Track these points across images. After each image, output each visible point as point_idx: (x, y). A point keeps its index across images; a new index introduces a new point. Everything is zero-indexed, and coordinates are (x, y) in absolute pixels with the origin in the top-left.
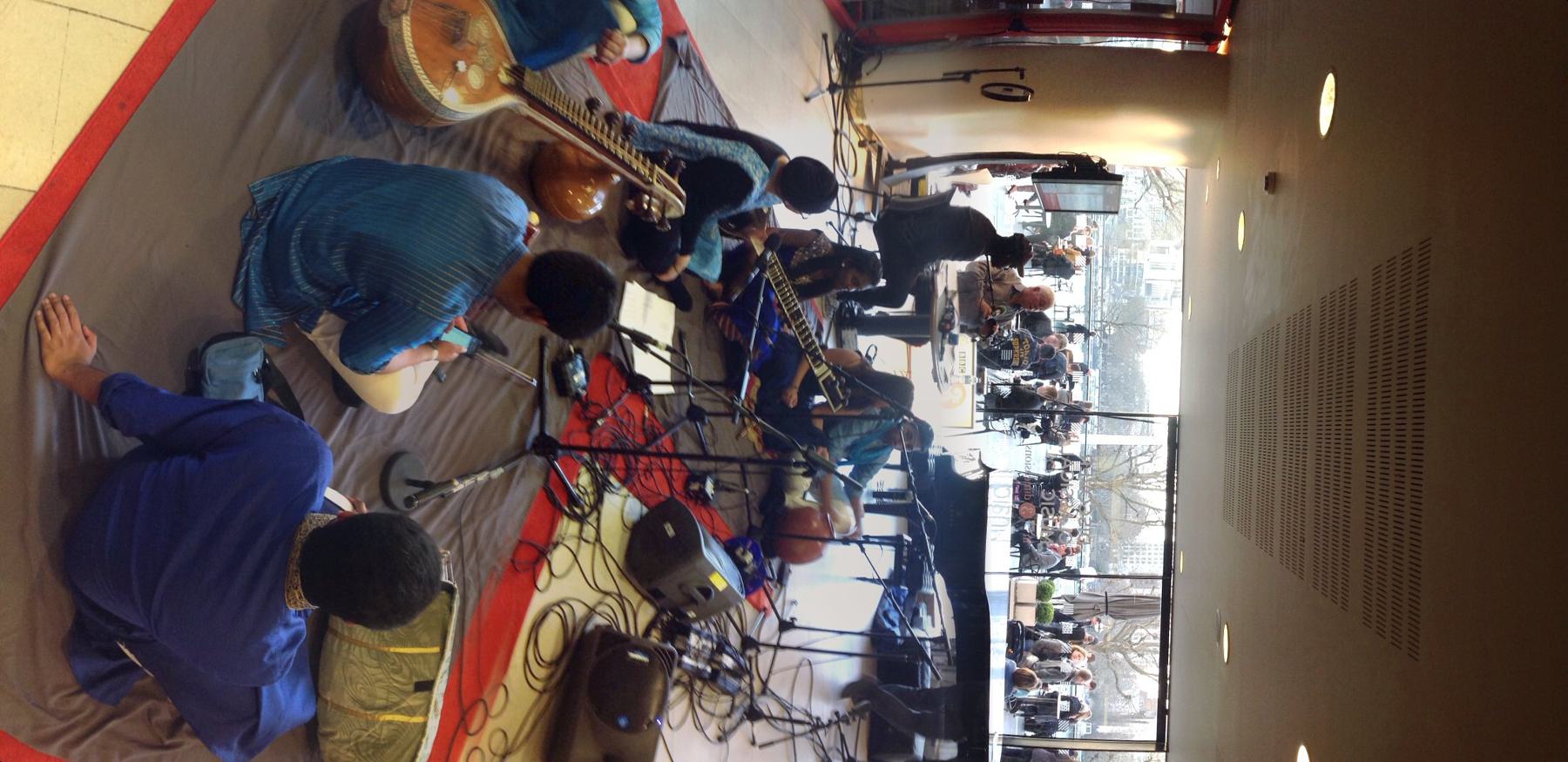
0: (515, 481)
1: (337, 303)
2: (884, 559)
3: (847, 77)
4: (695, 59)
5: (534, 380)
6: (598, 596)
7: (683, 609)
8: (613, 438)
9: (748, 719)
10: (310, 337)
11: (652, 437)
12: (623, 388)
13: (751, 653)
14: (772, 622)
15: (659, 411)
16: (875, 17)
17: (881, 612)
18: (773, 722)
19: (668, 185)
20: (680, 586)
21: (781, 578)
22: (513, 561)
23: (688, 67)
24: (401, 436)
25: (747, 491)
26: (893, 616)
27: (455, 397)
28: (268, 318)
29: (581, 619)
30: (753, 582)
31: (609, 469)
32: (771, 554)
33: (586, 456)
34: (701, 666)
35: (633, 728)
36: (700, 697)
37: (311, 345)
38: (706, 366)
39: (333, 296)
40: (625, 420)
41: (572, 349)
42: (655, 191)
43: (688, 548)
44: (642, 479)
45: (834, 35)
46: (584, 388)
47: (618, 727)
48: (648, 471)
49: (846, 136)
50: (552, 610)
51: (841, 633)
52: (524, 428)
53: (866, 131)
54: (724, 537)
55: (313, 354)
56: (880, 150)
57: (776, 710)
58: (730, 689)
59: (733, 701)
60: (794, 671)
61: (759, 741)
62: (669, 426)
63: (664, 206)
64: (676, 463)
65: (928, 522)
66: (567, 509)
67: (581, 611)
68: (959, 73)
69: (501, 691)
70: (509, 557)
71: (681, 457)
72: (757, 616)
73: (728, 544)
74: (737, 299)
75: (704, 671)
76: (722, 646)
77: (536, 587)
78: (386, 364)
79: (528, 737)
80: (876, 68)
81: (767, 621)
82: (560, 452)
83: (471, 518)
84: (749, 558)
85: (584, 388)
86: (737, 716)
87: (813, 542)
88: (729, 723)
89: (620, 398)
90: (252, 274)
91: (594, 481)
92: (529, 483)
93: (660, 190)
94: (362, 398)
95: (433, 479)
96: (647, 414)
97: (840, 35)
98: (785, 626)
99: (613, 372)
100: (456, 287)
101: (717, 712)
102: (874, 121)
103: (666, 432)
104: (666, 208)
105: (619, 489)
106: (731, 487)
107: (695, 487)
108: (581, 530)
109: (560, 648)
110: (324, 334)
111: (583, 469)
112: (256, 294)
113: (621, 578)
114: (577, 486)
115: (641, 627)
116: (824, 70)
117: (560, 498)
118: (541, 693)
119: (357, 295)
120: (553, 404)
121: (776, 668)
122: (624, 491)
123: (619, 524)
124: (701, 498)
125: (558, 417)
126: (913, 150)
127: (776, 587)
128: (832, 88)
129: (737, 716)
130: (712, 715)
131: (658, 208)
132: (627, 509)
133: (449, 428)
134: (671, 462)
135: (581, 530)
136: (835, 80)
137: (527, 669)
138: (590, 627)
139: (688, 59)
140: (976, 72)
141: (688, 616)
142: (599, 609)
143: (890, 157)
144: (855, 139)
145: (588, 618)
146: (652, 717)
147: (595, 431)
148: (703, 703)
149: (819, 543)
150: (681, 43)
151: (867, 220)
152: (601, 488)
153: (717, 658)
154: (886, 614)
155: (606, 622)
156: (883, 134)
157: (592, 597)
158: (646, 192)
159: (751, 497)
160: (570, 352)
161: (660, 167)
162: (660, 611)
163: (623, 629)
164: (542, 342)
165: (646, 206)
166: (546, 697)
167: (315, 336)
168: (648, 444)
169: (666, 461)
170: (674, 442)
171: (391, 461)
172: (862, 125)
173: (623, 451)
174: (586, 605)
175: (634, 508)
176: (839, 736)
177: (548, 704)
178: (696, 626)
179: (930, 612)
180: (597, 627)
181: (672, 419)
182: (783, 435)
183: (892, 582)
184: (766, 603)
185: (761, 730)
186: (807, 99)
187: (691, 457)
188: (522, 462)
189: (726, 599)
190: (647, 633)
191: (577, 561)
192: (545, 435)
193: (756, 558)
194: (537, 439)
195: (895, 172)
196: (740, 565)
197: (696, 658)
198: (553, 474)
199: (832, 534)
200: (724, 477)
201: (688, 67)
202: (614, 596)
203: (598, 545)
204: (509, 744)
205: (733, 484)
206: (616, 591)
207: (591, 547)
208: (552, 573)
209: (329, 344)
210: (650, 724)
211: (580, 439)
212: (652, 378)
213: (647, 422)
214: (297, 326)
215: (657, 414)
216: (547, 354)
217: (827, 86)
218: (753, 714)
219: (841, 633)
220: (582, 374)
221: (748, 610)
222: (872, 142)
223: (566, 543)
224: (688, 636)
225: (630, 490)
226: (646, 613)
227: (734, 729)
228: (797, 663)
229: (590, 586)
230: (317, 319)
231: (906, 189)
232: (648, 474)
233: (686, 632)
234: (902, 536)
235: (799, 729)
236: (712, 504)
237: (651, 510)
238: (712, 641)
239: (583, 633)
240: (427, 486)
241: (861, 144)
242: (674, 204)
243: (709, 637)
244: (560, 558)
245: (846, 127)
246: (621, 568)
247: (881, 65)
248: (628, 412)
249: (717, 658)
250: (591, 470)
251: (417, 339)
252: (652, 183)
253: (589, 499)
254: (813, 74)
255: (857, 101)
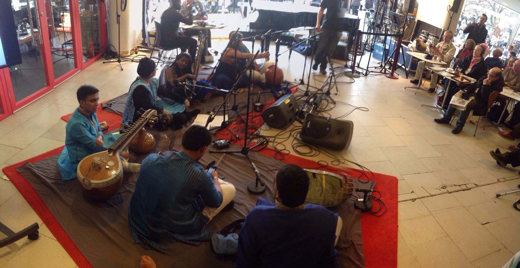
0: (256, 160)
1: (199, 209)
2: (284, 49)
3: (116, 56)
4: (109, 102)
5: (224, 154)
6: (291, 137)
7: (295, 112)
8: (242, 133)
9: (329, 95)
10: (211, 219)
11: (242, 121)
12: (226, 129)
13: (309, 94)
14: (301, 87)
15: (234, 119)
16: (98, 46)
17: (300, 52)
18: (330, 89)
19: (148, 113)
20: (288, 113)
21: (288, 83)
22: (281, 160)
23: (111, 105)
24: (242, 189)
25: (260, 92)
26: (302, 48)
27: (230, 174)
28: (204, 233)
29: (298, 141)
30: (288, 91)
31: (252, 134)
32: (280, 86)
33: (248, 140)
34: (312, 108)
35: (330, 126)
36: (322, 109)
37: (214, 218)
38: (219, 101)
39: (198, 209)
40: (237, 129)
41: (213, 144)
42: (149, 118)
43: (277, 110)
44: (255, 124)
45: (103, 60)
46: (226, 140)
47: (329, 131)
48: (252, 122)
49: (134, 58)
50: (295, 149)
51: (305, 65)
52: (239, 157)
53: (132, 51)
54: (274, 100)
55: (216, 218)
56: (139, 47)
57: (327, 87)
58: (320, 100)
59: (323, 99)
60: (316, 81)
61: (336, 92)
62: (239, 116)
63: (153, 116)
64: (250, 114)
65: (272, 31)
66: (265, 145)
67: (295, 142)
68: (117, 19)
69: (320, 162)
70: (279, 161)
71: (248, 114)
72: (299, 91)
73: (276, 99)
74: (196, 94)
75: (314, 107)
76: (307, 102)
77: (288, 154)
78: (219, 192)
79: (334, 156)
80: (114, 47)
81: (300, 88)
82: (247, 147)
83: (266, 167)
84: (280, 92)
85: (226, 140)
86: (328, 98)
87: (276, 71)
88: (330, 101)
89: (230, 131)
90: (189, 238)
91: (256, 138)
92: (257, 156)
93: (149, 116)
94: (230, 201)
95: (255, 179)
96: (235, 123)
97: (104, 58)
98: (302, 82)
99: (222, 133)
100: (195, 170)
101: (327, 104)
102: (130, 48)
103: (240, 117)
104: (154, 115)
105: (259, 131)
106: (258, 97)
107: (258, 109)
108: (271, 142)
109: (306, 147)
110: (210, 214)
111: (252, 141)
112: (196, 237)
113: (285, 131)
114: (258, 143)
115: (301, 125)
116: (114, 64)
117: (261, 147)
118: (320, 152)
119: (196, 202)
120: (230, 150)
121: (314, 86)
122: (259, 130)
123: (266, 132)
124: (262, 107)
125: (235, 148)
126: (140, 35)
127: (290, 85)
128: (119, 61)
129: (328, 98)
130: (327, 105)
131: (154, 118)
132: (265, 129)
133: (240, 175)
134: (250, 116)
135: (271, 142)
136: (117, 60)
137: (314, 156)
138: (300, 139)
139: (109, 104)
140: (117, 13)
141: (297, 111)
142: (295, 136)
143: (141, 44)
144: (135, 55)
145: (297, 140)
146: (327, 121)
147: (240, 138)
148: (324, 108)
149: (277, 70)
150: (104, 106)
151: (166, 54)
152: (258, 136)
153: (310, 103)
154: (301, 51)
155: (299, 134)
156: (134, 45)
157: (291, 139)
158: (149, 121)
159: (262, 91)
160: (214, 145)
161: (142, 115)
162: (296, 119)
163: (300, 130)
164: (211, 152)
165: (153, 121)
166: (321, 151)
167: (211, 217)
168: (244, 123)
169: (249, 118)
170: (244, 115)
171: (251, 192)
172: (130, 52)
173: (246, 130)
174: (293, 141)
175: (264, 127)
176: (337, 69)
177: (324, 150)
178: (301, 109)
179: (302, 36)
180: (300, 137)
181: (236, 115)
182: (241, 76)
183: (291, 48)
184: (295, 88)
185: (333, 91)
186: (122, 70)
187: (248, 110)
188: (250, 158)
189: (293, 99)
190: (302, 123)
191: (281, 143)
192: (241, 151)
193: (281, 90)
194: (243, 154)
195: (146, 42)
196: (283, 95)
197: (310, 109)
198: (253, 149)
199: (274, 66)
200: (255, 100)
201: (111, 105)
202: (291, 132)
203: (276, 137)
204: (335, 160)
205: (257, 97)
206: (290, 132)
207: (276, 139)
208: (284, 150)
209: (213, 212)
210: (328, 121)
211: (243, 142)
212: (223, 120)
213: (237, 123)
214: (207, 224)
215: (234, 120)
216: (215, 151)
217: (118, 63)
218: (328, 93)
219: (305, 65)
220: (222, 141)
221: (297, 94)
222: (136, 50)
223: (275, 146)
224: (304, 111)
225: (259, 128)
226: (297, 124)
227: (332, 100)
228: (314, 80)
229: (288, 139)
230: (204, 216)
231: (152, 40)
232: (254, 122)
233: (302, 112)
234: (276, 43)
235: (333, 80)
236: (263, 104)
237: (265, 121)
238: (305, 104)
239: (303, 141)
240: (258, 180)
241: (136, 53)
242: (153, 113)
243: (304, 105)
244: (280, 147)
245: (131, 58)
246: (282, 131)
247: (113, 45)
248: (234, 128)
249: (310, 103)
250: (253, 139)
251: (211, 181)
252: (146, 118)
253: (262, 140)
254: (115, 67)
255: (123, 53)
